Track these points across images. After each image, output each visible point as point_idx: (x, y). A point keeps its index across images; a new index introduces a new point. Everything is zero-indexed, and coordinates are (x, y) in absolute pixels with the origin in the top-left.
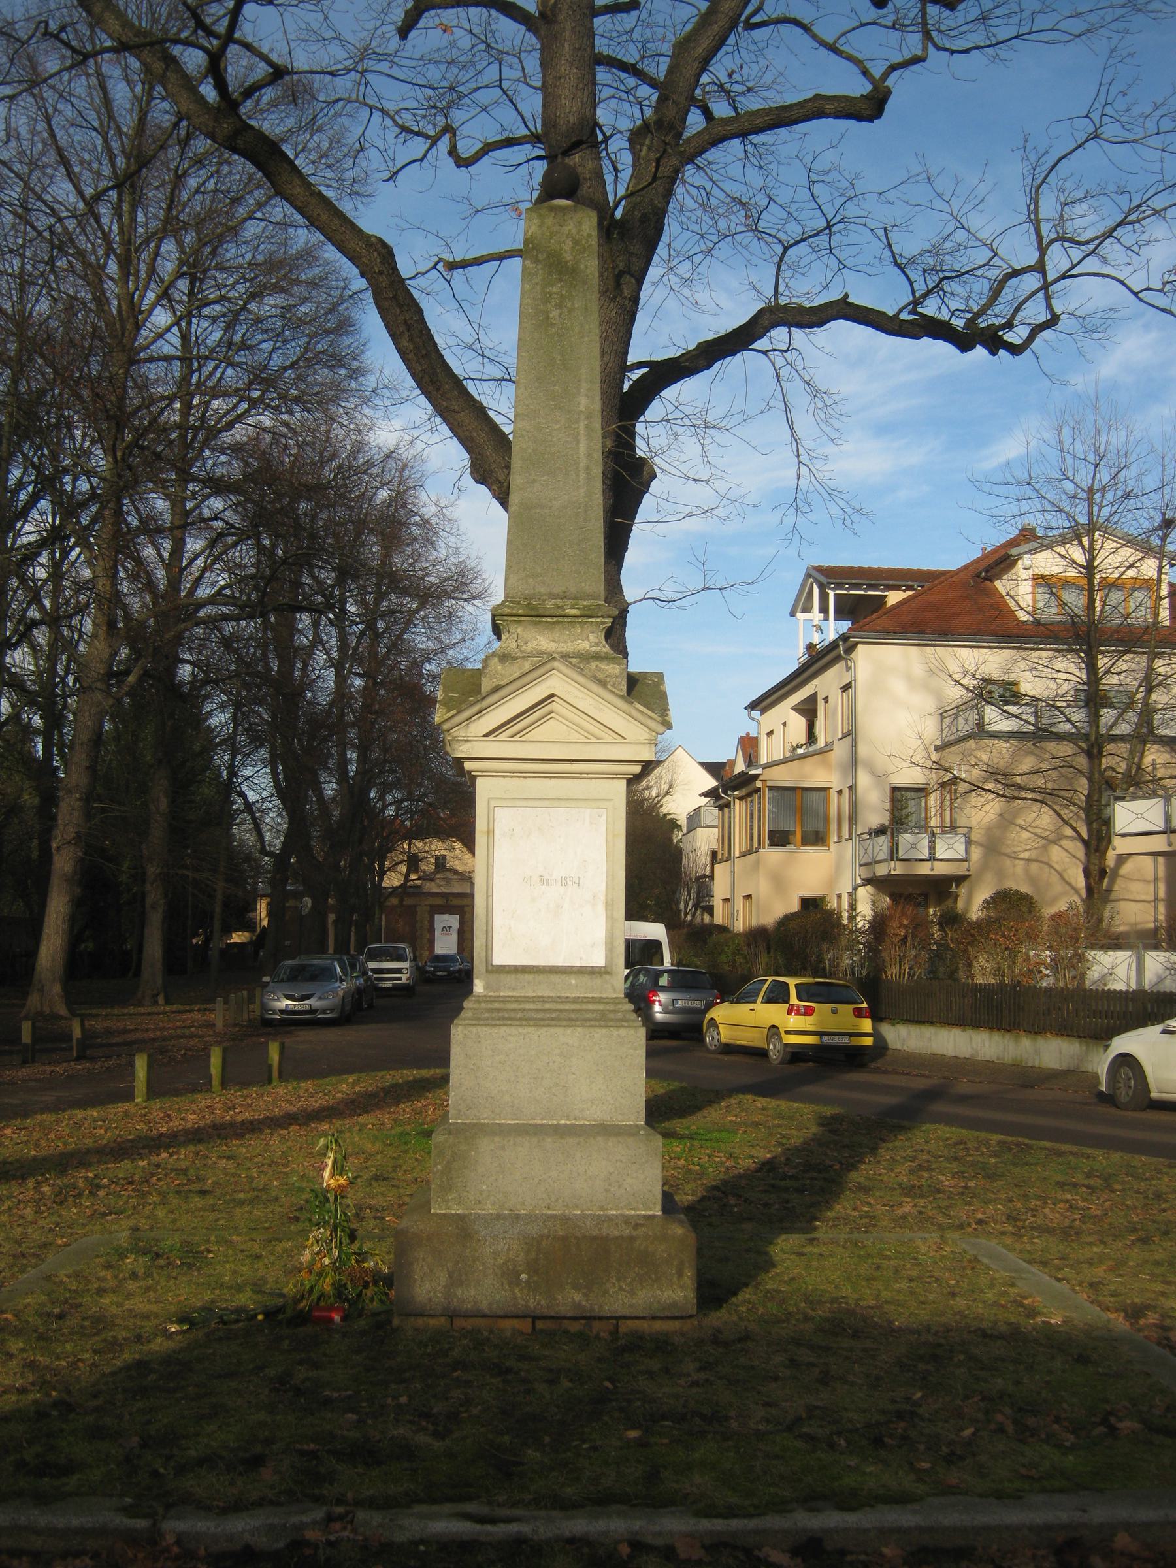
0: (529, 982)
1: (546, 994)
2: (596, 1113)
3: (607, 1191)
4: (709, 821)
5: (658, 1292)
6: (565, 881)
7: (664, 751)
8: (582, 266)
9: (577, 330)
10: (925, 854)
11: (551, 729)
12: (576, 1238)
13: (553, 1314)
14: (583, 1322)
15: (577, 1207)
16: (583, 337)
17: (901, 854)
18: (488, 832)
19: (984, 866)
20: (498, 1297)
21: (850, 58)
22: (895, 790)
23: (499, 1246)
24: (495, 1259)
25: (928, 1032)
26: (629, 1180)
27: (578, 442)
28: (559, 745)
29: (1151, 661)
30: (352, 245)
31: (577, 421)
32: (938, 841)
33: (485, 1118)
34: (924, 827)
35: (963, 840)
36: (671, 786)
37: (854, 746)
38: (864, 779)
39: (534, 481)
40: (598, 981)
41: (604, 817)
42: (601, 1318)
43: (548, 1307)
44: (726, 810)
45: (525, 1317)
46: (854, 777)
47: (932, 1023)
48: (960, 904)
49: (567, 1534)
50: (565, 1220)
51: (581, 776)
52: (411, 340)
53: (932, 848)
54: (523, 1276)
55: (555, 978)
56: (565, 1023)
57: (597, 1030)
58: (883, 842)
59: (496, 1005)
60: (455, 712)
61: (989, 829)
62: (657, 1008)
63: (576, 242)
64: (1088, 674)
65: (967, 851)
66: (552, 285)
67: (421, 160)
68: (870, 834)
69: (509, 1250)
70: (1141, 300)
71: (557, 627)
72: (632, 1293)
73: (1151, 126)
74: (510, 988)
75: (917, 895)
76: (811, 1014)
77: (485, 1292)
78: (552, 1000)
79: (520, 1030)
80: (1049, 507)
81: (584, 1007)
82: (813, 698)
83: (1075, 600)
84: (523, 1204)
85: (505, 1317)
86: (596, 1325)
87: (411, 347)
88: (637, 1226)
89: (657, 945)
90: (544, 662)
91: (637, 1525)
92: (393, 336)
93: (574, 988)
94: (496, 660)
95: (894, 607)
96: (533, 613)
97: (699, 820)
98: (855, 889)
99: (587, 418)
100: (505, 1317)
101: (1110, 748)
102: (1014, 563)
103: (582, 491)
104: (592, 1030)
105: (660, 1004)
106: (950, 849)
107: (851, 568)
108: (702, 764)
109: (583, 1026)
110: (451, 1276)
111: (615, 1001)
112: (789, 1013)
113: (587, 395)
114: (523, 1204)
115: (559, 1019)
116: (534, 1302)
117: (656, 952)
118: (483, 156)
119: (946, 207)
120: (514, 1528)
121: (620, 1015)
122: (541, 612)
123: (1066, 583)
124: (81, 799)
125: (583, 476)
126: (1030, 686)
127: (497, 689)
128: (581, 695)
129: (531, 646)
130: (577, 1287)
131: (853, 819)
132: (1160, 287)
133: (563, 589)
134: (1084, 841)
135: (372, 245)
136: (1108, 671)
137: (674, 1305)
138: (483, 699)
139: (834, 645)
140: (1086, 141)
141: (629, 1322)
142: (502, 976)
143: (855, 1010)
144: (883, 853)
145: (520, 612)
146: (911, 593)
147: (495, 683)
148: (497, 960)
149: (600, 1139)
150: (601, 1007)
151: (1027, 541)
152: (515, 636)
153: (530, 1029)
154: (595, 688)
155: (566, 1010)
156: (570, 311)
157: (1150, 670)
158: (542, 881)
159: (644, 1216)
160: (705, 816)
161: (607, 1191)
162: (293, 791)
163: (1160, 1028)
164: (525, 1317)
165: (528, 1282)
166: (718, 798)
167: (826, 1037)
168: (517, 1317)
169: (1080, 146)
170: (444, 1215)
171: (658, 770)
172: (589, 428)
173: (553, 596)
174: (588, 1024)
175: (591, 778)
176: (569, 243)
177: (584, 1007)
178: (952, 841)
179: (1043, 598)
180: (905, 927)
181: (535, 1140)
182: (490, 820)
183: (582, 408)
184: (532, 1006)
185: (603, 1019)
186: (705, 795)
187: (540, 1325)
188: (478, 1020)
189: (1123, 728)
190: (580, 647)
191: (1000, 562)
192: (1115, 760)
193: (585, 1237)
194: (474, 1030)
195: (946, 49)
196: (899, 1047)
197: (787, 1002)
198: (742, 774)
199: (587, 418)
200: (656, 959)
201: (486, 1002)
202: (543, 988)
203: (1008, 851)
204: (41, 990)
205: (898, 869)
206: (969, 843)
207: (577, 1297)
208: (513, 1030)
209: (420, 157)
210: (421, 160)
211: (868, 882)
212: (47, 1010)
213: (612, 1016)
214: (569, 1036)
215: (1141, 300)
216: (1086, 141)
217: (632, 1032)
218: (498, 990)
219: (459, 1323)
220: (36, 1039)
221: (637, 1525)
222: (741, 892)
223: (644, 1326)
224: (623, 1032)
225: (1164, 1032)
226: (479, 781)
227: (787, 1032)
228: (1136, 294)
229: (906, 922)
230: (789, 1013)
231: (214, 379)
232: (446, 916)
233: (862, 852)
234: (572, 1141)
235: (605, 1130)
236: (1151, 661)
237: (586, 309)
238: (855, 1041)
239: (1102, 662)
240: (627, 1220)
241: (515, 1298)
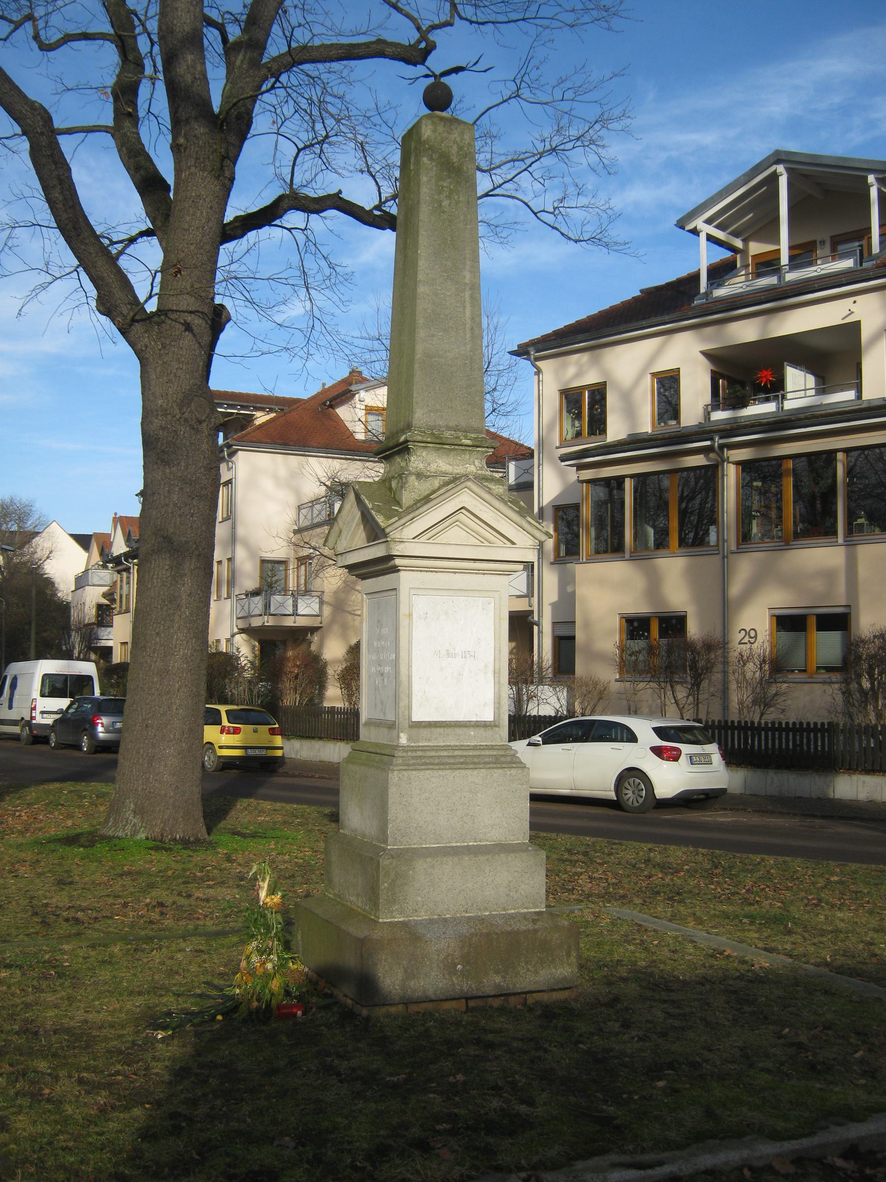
0: (441, 734)
1: (452, 744)
2: (495, 835)
3: (508, 895)
4: (96, 581)
5: (554, 970)
6: (465, 654)
7: (42, 525)
8: (465, 168)
9: (462, 217)
10: (290, 610)
12: (497, 934)
13: (480, 994)
14: (502, 998)
15: (486, 909)
16: (466, 224)
17: (272, 610)
19: (333, 621)
20: (441, 985)
21: (408, 16)
22: (263, 562)
23: (442, 945)
24: (438, 955)
25: (317, 744)
26: (523, 886)
27: (464, 308)
28: (469, 547)
31: (464, 291)
32: (299, 601)
33: (414, 844)
34: (285, 591)
35: (318, 600)
36: (51, 552)
37: (234, 527)
38: (241, 554)
39: (434, 335)
40: (490, 733)
41: (493, 604)
42: (514, 994)
43: (477, 989)
44: (125, 574)
45: (460, 998)
46: (233, 552)
47: (321, 738)
48: (313, 648)
49: (703, 1168)
50: (482, 920)
51: (479, 571)
52: (62, 193)
53: (295, 606)
55: (458, 731)
56: (471, 766)
57: (495, 770)
58: (257, 603)
59: (419, 753)
60: (396, 518)
61: (335, 592)
62: (100, 729)
63: (461, 149)
65: (320, 609)
66: (444, 180)
67: (5, 40)
68: (247, 595)
69: (449, 947)
70: (538, 218)
72: (536, 972)
73: (558, 95)
74: (427, 740)
76: (239, 733)
77: (431, 981)
79: (440, 772)
81: (483, 753)
84: (448, 910)
85: (446, 1000)
86: (512, 999)
87: (61, 198)
88: (534, 921)
89: (90, 678)
91: (745, 1153)
92: (45, 188)
93: (473, 738)
94: (414, 477)
96: (438, 441)
97: (87, 580)
98: (233, 636)
99: (471, 289)
100: (446, 1000)
102: (354, 395)
104: (492, 771)
105: (103, 726)
106: (308, 607)
107: (233, 393)
108: (71, 535)
110: (406, 971)
112: (222, 732)
113: (470, 271)
114: (448, 910)
115: (467, 764)
117: (87, 685)
118: (63, 44)
119: (389, 132)
120: (667, 1169)
122: (444, 441)
128: (484, 509)
129: (433, 467)
130: (497, 972)
131: (231, 583)
132: (552, 210)
133: (456, 423)
135: (35, 110)
137: (565, 979)
140: (510, 98)
142: (421, 730)
143: (270, 729)
145: (429, 440)
146: (274, 414)
148: (418, 715)
149: (502, 855)
150: (495, 753)
153: (447, 772)
156: (457, 203)
158: (448, 654)
159: (535, 913)
160: (92, 577)
161: (508, 895)
163: (526, 741)
164: (460, 998)
165: (462, 971)
167: (249, 750)
169: (504, 101)
170: (390, 922)
171: (37, 539)
173: (449, 428)
174: (488, 766)
176: (455, 148)
177: (483, 753)
178: (310, 602)
180: (298, 666)
181: (456, 859)
182: (410, 606)
183: (467, 281)
184: (445, 753)
187: (472, 1004)
190: (469, 470)
191: (342, 393)
193: (502, 933)
194: (406, 773)
195: (466, 19)
196: (293, 756)
197: (220, 724)
199: (471, 289)
200: (86, 690)
201: (411, 751)
202: (451, 739)
203: (350, 609)
205: (270, 622)
206: (322, 603)
207: (498, 979)
208: (435, 773)
209: (4, 37)
210: (5, 40)
211: (242, 631)
213: (503, 759)
214: (475, 776)
215: (538, 218)
216: (510, 98)
217: (520, 771)
218: (418, 741)
219: (413, 1008)
221: (745, 1153)
223: (545, 997)
225: (530, 744)
227: (221, 747)
228: (535, 214)
229: (298, 663)
230: (222, 732)
233: (239, 608)
234: (482, 858)
235: (503, 848)
237: (468, 202)
238: (270, 753)
240: (524, 916)
241: (453, 985)
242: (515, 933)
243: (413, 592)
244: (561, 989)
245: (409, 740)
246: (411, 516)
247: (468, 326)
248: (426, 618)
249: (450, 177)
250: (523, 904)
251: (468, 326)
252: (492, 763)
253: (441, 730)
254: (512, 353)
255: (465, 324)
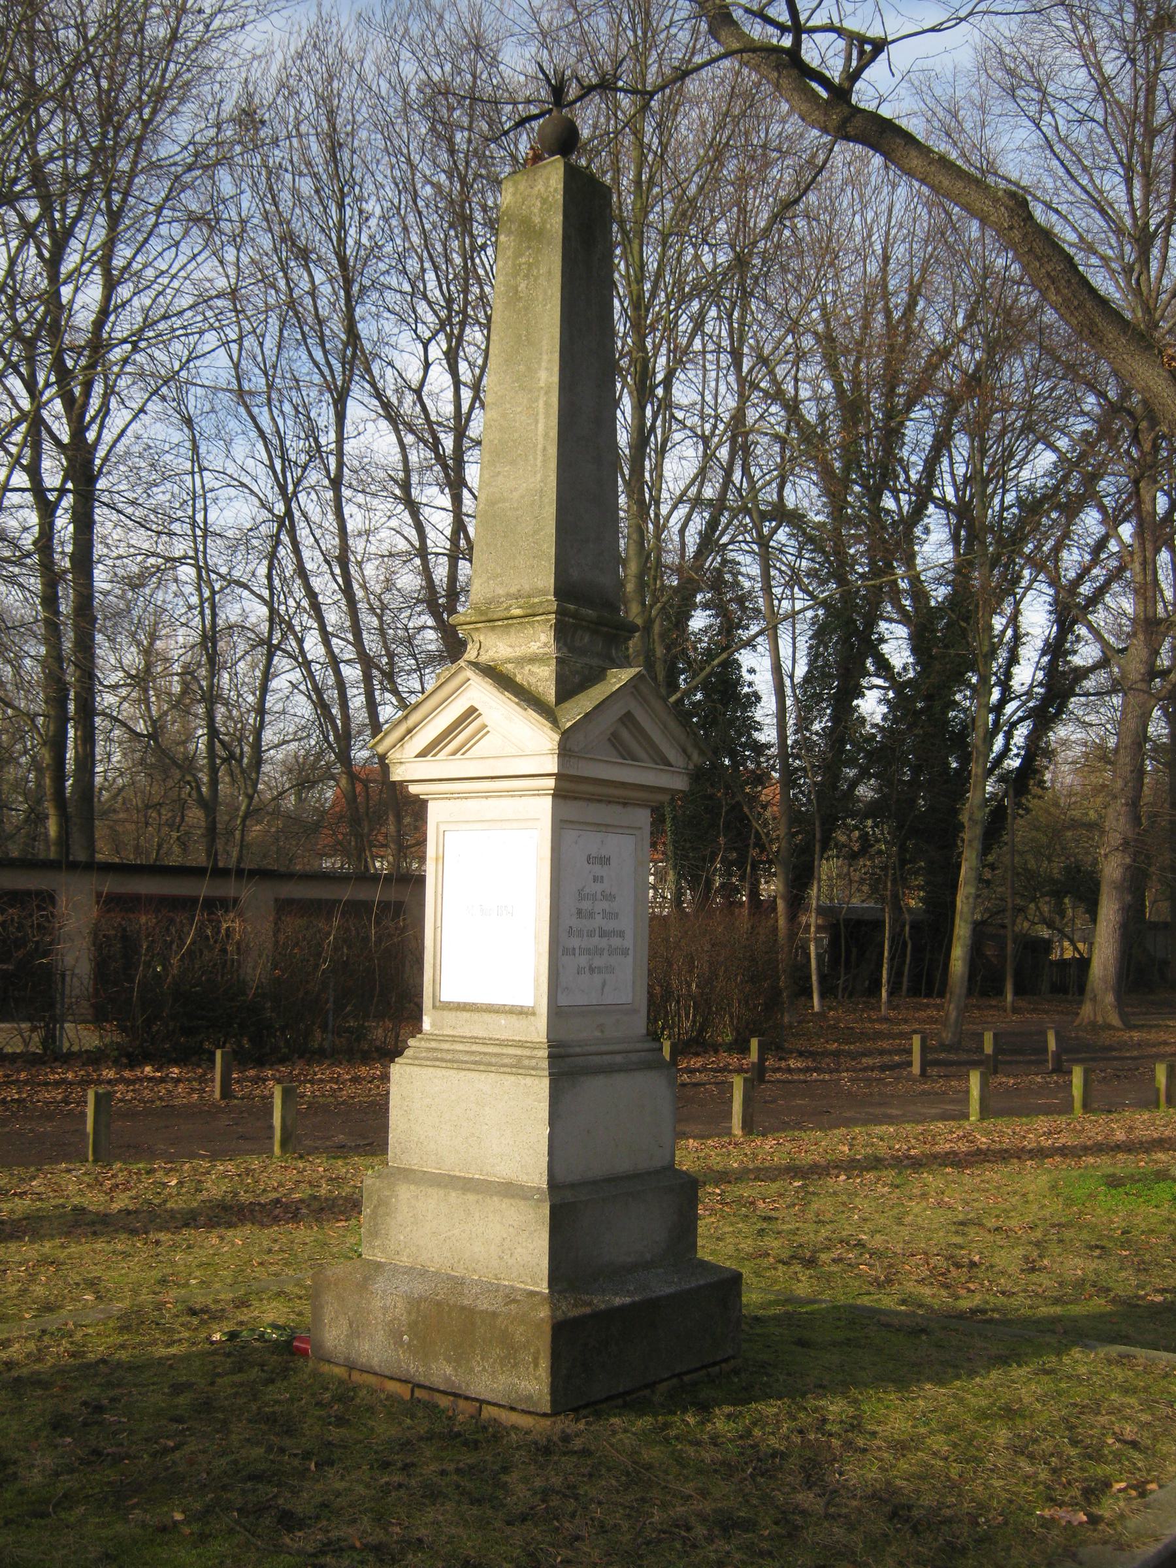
3: (501, 1258)
13: (427, 1384)
27: (537, 422)
30: (978, 205)
42: (467, 1398)
45: (406, 1382)
50: (458, 1283)
55: (487, 1017)
71: (513, 630)
77: (376, 1349)
81: (505, 1050)
85: (391, 1378)
86: (462, 1403)
93: (504, 1028)
103: (539, 477)
111: (534, 1046)
116: (413, 1367)
121: (533, 1062)
122: (491, 616)
124: (1127, 804)
125: (540, 458)
130: (448, 1360)
137: (529, 1398)
141: (490, 1408)
142: (445, 1013)
148: (446, 996)
150: (519, 1052)
164: (406, 1382)
168: (400, 1380)
172: (546, 404)
177: (505, 1050)
181: (442, 1192)
183: (542, 384)
185: (518, 1067)
187: (418, 1393)
188: (418, 1062)
204: (1094, 999)
212: (1100, 1020)
214: (483, 1082)
219: (356, 1376)
220: (998, 1049)
226: (430, 805)
234: (471, 1197)
241: (399, 1361)
242: (469, 1313)
244: (523, 1411)
245: (432, 1025)
249: (529, 248)
250: (519, 1275)
251: (540, 446)
253: (466, 1015)
255: (535, 446)
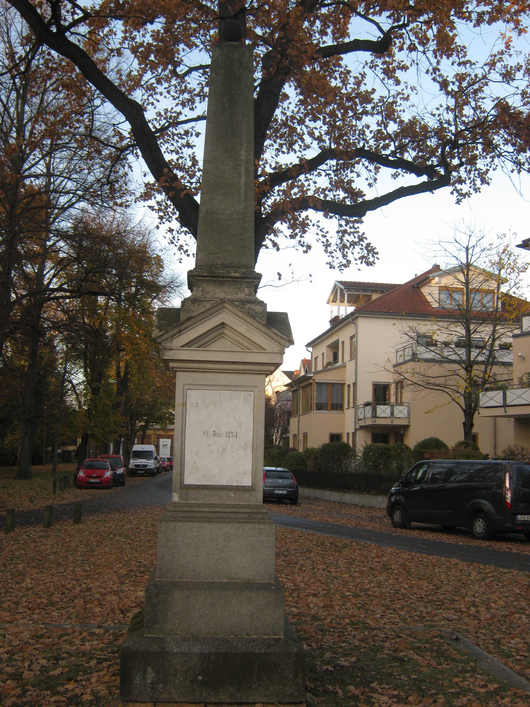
1: (216, 502)
6: (229, 434)
11: (221, 344)
18: (183, 405)
27: (240, 177)
29: (494, 327)
40: (246, 495)
54: (200, 678)
55: (222, 493)
59: (186, 509)
60: (164, 332)
64: (466, 332)
75: (386, 435)
78: (219, 505)
79: (200, 524)
80: (449, 254)
82: (337, 342)
83: (460, 298)
90: (219, 306)
93: (232, 499)
95: (375, 300)
96: (212, 275)
101: (475, 367)
109: (238, 522)
123: (457, 290)
125: (242, 197)
126: (441, 337)
127: (189, 319)
128: (240, 323)
134: (463, 410)
136: (475, 331)
138: (181, 324)
139: (347, 317)
144: (369, 415)
145: (205, 274)
147: (189, 315)
148: (188, 481)
151: (436, 271)
152: (201, 289)
154: (248, 319)
155: (227, 512)
157: (494, 331)
159: (274, 639)
162: (94, 380)
164: (199, 703)
166: (292, 387)
170: (151, 637)
175: (245, 373)
179: (443, 296)
184: (207, 509)
186: (286, 386)
189: (480, 358)
191: (423, 280)
192: (477, 371)
194: (172, 524)
198: (304, 376)
214: (228, 528)
217: (267, 526)
222: (302, 432)
224: (262, 526)
231: (61, 187)
232: (165, 440)
235: (248, 586)
236: (494, 327)
239: (472, 327)
243: (186, 387)
245: (180, 498)
246: (177, 330)
247: (242, 190)
248: (197, 406)
251: (242, 190)
252: (246, 518)
254: (518, 246)
